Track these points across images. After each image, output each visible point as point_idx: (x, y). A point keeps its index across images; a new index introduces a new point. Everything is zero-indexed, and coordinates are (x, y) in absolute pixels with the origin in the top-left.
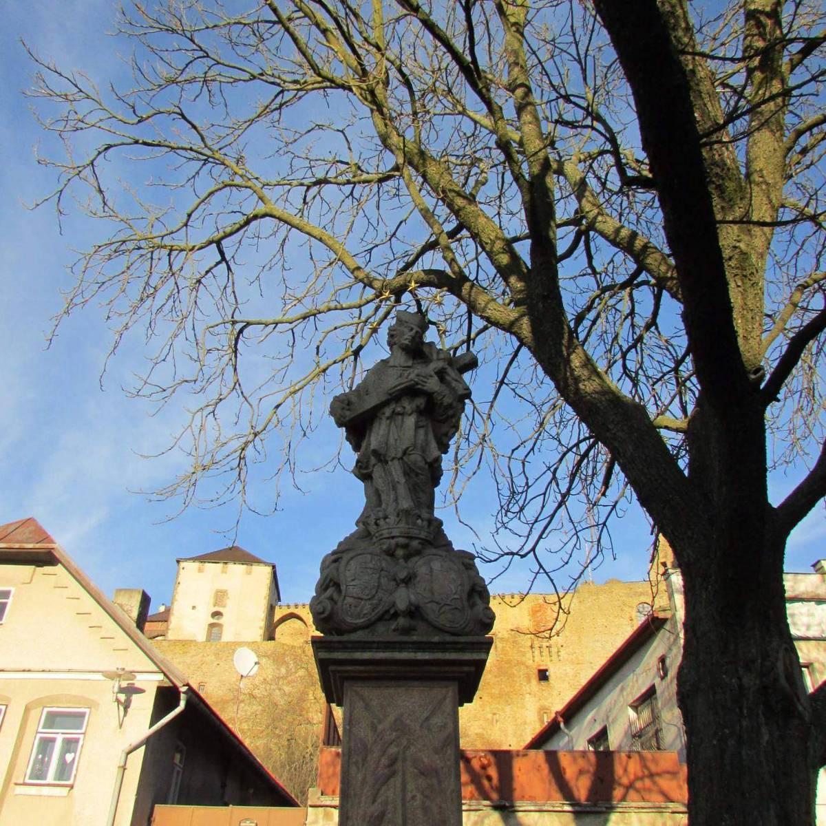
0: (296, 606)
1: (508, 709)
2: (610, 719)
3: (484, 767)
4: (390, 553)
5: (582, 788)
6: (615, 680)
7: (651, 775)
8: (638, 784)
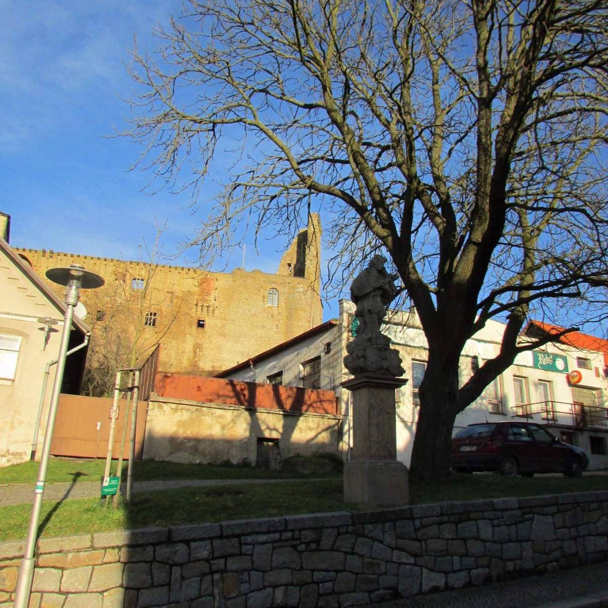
0: (24, 250)
1: (174, 342)
2: (286, 368)
3: (242, 390)
4: (380, 350)
5: (288, 404)
6: (294, 348)
7: (321, 401)
8: (314, 405)
